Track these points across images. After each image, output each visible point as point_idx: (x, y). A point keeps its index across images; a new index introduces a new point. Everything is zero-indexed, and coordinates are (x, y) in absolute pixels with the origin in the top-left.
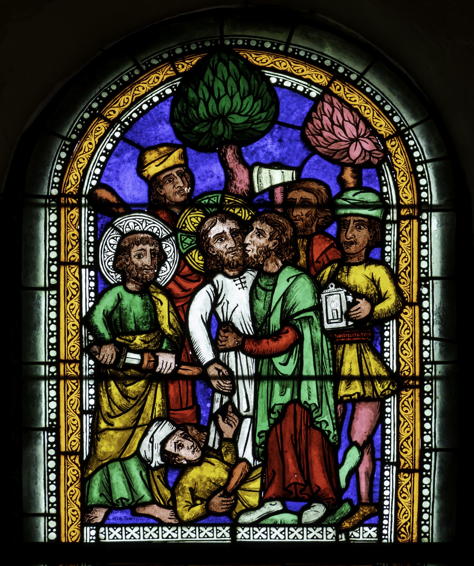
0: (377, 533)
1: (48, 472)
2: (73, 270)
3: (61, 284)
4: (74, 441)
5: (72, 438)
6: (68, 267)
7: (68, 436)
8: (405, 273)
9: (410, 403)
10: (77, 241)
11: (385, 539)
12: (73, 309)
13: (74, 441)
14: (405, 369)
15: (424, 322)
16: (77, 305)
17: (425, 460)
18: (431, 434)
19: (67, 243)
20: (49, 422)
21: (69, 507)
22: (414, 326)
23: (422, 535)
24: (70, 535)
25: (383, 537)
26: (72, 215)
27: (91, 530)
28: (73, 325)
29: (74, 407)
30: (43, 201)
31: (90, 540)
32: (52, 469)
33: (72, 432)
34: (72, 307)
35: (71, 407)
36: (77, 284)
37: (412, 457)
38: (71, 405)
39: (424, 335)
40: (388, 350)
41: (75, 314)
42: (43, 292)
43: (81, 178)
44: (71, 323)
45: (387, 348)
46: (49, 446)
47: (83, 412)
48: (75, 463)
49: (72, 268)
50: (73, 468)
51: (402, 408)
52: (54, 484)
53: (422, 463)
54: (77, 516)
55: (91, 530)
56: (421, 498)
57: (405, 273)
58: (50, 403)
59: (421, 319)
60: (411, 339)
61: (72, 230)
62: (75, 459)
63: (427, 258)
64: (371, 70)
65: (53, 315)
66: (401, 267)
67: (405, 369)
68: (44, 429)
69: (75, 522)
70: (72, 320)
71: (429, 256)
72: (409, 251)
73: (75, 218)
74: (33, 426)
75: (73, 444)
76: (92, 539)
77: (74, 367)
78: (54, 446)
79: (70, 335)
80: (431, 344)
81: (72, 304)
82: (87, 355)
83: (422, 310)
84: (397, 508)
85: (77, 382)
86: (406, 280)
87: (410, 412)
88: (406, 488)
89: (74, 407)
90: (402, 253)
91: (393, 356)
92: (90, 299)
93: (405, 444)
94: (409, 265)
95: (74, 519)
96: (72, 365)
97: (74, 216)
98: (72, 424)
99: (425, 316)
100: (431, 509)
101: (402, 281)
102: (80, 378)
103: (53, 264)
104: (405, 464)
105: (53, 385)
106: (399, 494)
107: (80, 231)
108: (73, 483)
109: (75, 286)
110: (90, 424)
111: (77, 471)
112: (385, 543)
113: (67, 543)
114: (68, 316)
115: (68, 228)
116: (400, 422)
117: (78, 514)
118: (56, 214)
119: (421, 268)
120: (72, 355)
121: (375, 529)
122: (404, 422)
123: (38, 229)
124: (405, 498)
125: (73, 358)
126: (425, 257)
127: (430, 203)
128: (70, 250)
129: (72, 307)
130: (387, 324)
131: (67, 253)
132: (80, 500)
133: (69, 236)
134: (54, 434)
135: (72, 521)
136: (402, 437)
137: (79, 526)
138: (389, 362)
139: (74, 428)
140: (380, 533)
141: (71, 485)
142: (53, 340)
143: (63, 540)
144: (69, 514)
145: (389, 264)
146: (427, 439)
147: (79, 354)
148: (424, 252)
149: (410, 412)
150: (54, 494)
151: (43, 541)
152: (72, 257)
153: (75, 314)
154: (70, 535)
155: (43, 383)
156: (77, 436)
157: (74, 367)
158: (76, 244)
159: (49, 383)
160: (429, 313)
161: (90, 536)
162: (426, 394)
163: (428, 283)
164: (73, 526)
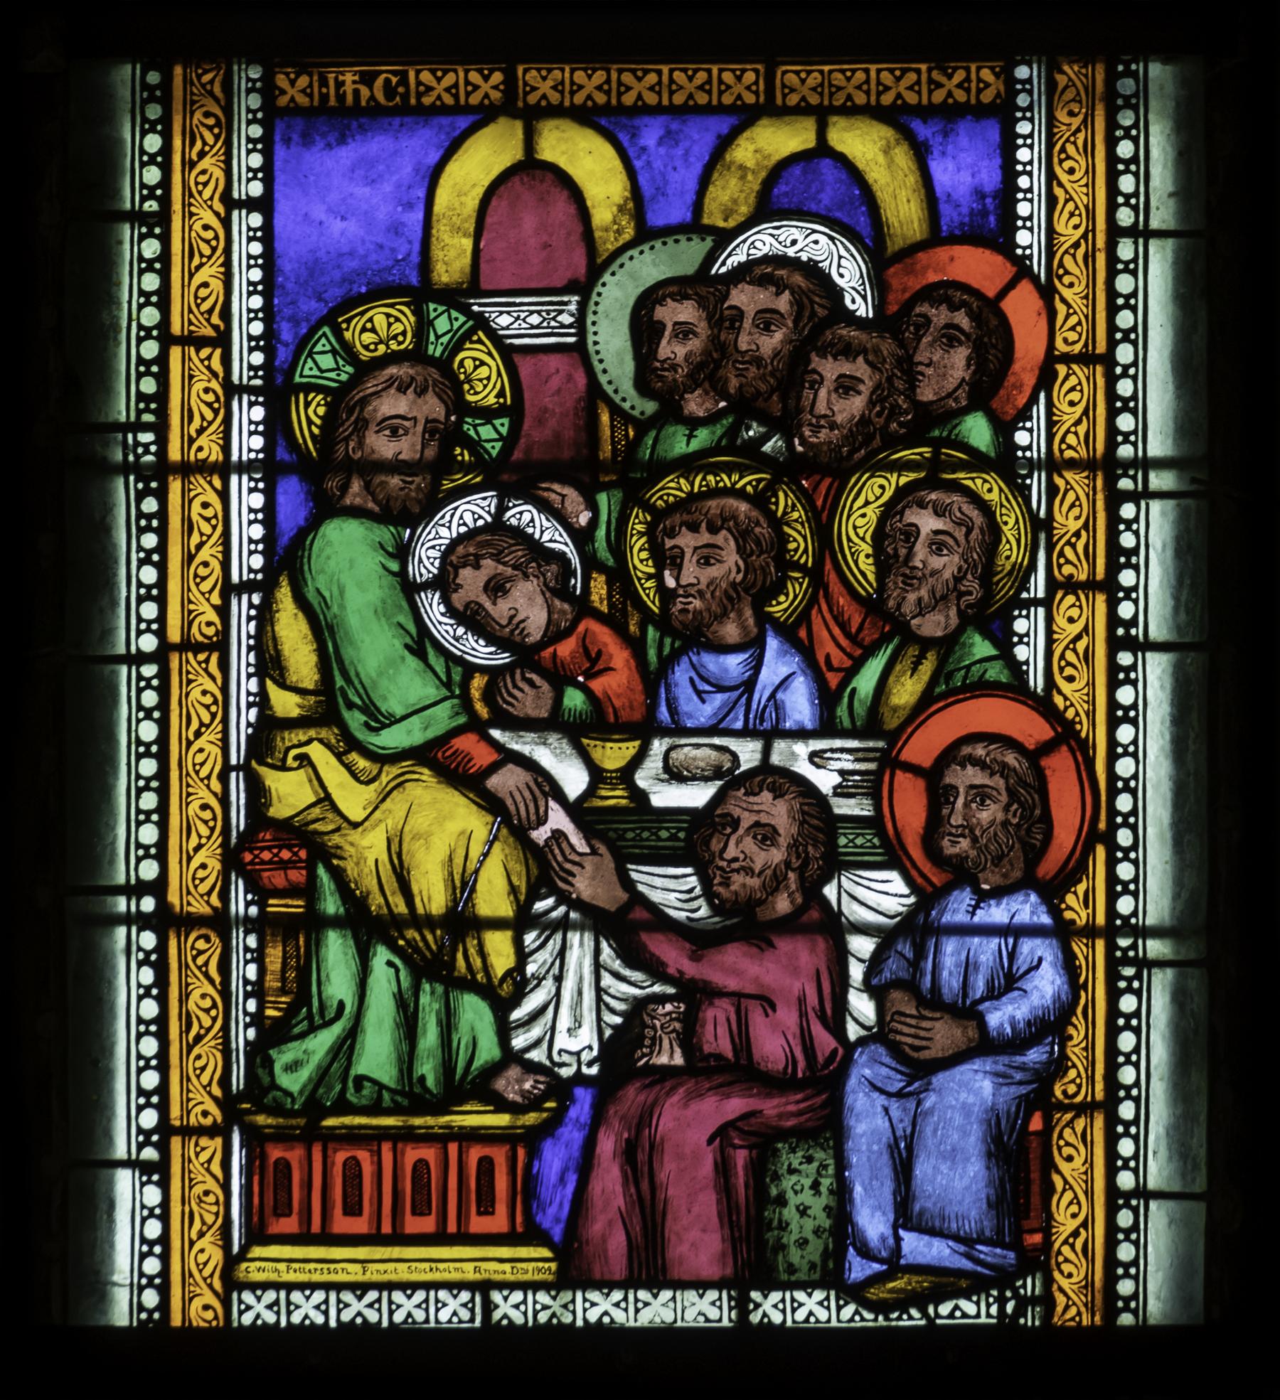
4: (1071, 620)
5: (204, 555)
7: (1088, 531)
9: (1081, 652)
12: (202, 880)
13: (1071, 620)
14: (1068, 1316)
15: (1120, 784)
17: (1122, 984)
18: (1137, 205)
20: (138, 1097)
21: (192, 494)
22: (183, 966)
23: (1120, 1163)
27: (251, 405)
29: (205, 1078)
30: (121, 904)
31: (250, 378)
33: (198, 540)
37: (1086, 297)
39: (1119, 954)
42: (124, 669)
44: (199, 1109)
45: (1025, 219)
46: (142, 1028)
47: (229, 589)
50: (1073, 178)
52: (1121, 295)
54: (214, 522)
55: (251, 405)
57: (1072, 1247)
61: (198, 983)
63: (1133, 405)
65: (151, 1080)
67: (1068, 1316)
71: (1141, 261)
72: (1086, 706)
73: (206, 1065)
76: (256, 377)
77: (209, 358)
79: (1081, 652)
80: (1142, 189)
81: (1074, 1216)
84: (1052, 201)
86: (1075, 566)
87: (1078, 1161)
88: (1075, 650)
91: (1039, 195)
94: (1084, 1225)
95: (1071, 439)
96: (205, 352)
97: (204, 755)
98: (201, 819)
99: (150, 316)
100: (1142, 199)
101: (1066, 1268)
102: (224, 469)
103: (150, 1253)
104: (1067, 1307)
106: (1056, 160)
110: (249, 725)
111: (213, 695)
113: (188, 1331)
118: (155, 998)
120: (201, 587)
123: (116, 355)
124: (1071, 679)
126: (1129, 434)
133: (191, 813)
134: (155, 1178)
139: (206, 529)
141: (201, 431)
143: (176, 1321)
144: (195, 517)
146: (151, 248)
148: (1125, 695)
150: (155, 333)
155: (127, 229)
157: (209, 358)
159: (138, 673)
161: (251, 422)
163: (1134, 67)
164: (203, 852)
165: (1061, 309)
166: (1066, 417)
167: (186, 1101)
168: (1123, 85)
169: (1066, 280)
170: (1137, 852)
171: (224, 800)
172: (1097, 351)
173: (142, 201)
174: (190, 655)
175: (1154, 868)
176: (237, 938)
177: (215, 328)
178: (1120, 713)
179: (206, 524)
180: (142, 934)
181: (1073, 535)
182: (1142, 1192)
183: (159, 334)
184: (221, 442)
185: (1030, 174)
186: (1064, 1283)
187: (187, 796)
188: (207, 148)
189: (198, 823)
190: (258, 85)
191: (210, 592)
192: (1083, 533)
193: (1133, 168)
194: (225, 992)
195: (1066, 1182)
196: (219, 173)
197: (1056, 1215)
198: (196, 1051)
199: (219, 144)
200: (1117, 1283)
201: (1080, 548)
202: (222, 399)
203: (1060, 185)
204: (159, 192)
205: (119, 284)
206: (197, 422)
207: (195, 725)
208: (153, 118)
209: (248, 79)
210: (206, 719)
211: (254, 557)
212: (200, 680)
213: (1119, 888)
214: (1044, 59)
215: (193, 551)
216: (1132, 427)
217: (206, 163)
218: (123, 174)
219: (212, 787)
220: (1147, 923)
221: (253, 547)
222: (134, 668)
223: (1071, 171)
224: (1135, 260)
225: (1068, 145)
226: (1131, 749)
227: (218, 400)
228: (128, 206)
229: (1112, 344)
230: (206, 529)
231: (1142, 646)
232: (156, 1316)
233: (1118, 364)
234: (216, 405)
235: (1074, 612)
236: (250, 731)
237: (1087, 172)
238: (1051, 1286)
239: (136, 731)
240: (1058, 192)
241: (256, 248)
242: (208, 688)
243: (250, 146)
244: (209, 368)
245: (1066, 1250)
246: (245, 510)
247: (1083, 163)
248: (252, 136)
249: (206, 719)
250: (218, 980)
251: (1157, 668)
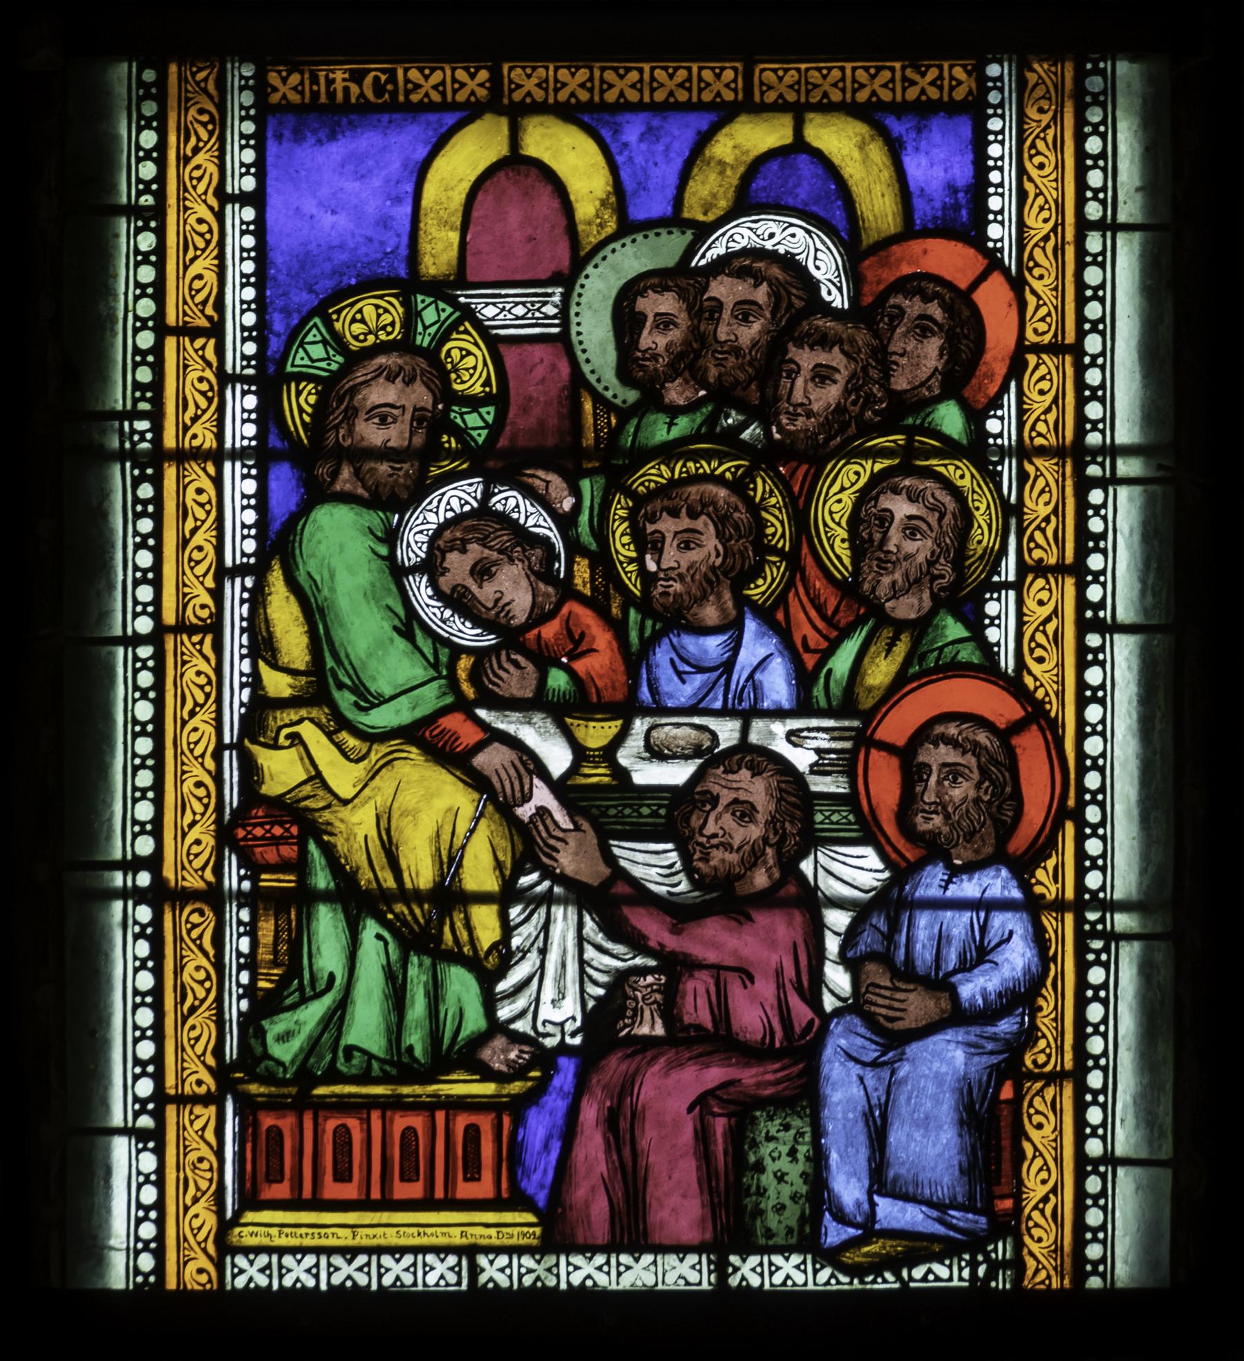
7: (1057, 517)
9: (1050, 634)
12: (197, 855)
14: (1038, 1279)
15: (1088, 762)
17: (1091, 957)
18: (1105, 200)
20: (134, 1067)
21: (187, 480)
22: (178, 939)
23: (1088, 1131)
27: (244, 393)
29: (199, 1048)
30: (118, 879)
31: (243, 368)
33: (193, 525)
38: (192, 1042)
39: (1087, 927)
42: (120, 651)
43: (215, 965)
44: (193, 1078)
45: (996, 213)
46: (138, 1000)
47: (222, 573)
52: (1089, 287)
54: (208, 507)
55: (244, 393)
57: (1042, 1212)
61: (193, 956)
63: (1101, 394)
65: (146, 1049)
67: (1038, 1279)
71: (1109, 254)
72: (1055, 686)
76: (248, 366)
77: (203, 348)
80: (1110, 184)
81: (1044, 1182)
84: (1022, 196)
87: (1048, 1129)
88: (1044, 632)
91: (1010, 190)
94: (1054, 1190)
95: (1041, 427)
96: (199, 342)
97: (198, 734)
98: (195, 796)
99: (146, 307)
100: (1110, 193)
101: (1036, 1232)
102: (218, 456)
103: (146, 1218)
104: (1037, 1271)
106: (1026, 156)
107: (218, 778)
109: (202, 680)
110: (242, 704)
111: (207, 676)
113: (183, 1294)
118: (150, 970)
120: (195, 571)
123: (112, 345)
124: (1040, 660)
126: (1097, 422)
133: (185, 790)
134: (151, 1145)
139: (201, 514)
141: (195, 419)
143: (171, 1284)
144: (189, 503)
148: (1093, 676)
150: (150, 324)
155: (123, 222)
157: (203, 348)
159: (135, 654)
161: (244, 410)
163: (1102, 65)
164: (197, 828)
165: (1031, 301)
166: (1036, 406)
167: (180, 1071)
168: (1092, 83)
169: (1036, 272)
170: (1105, 829)
172: (1067, 342)
173: (138, 196)
175: (1121, 844)
176: (231, 912)
177: (209, 318)
178: (1088, 693)
179: (201, 510)
180: (138, 908)
181: (1043, 520)
182: (1110, 1159)
183: (155, 325)
184: (215, 430)
185: (1001, 169)
186: (1035, 1247)
187: (182, 774)
188: (201, 144)
189: (193, 800)
190: (251, 82)
191: (204, 575)
192: (1053, 518)
193: (1101, 163)
194: (219, 965)
195: (1036, 1149)
196: (212, 169)
197: (1026, 1182)
198: (190, 1022)
199: (213, 140)
200: (1085, 1247)
201: (1050, 533)
202: (216, 388)
203: (1031, 180)
204: (154, 187)
205: (115, 276)
206: (191, 411)
207: (189, 704)
209: (241, 77)
210: (201, 699)
211: (247, 541)
212: (195, 661)
213: (1088, 863)
214: (1015, 57)
215: (188, 536)
216: (1100, 415)
217: (200, 158)
218: (120, 169)
219: (206, 765)
220: (1115, 897)
221: (246, 532)
222: (130, 650)
223: (1041, 166)
224: (1103, 253)
225: (1038, 141)
226: (1100, 728)
227: (211, 389)
228: (124, 200)
229: (1081, 335)
230: (201, 514)
231: (1110, 628)
232: (152, 1279)
233: (1086, 354)
234: (210, 394)
235: (1044, 595)
236: (243, 710)
237: (1056, 167)
238: (1021, 1251)
239: (133, 710)
240: (1029, 186)
241: (249, 241)
242: (202, 669)
243: (243, 142)
244: (203, 358)
246: (238, 496)
247: (1053, 159)
248: (245, 132)
249: (201, 699)
250: (212, 953)
251: (1124, 650)
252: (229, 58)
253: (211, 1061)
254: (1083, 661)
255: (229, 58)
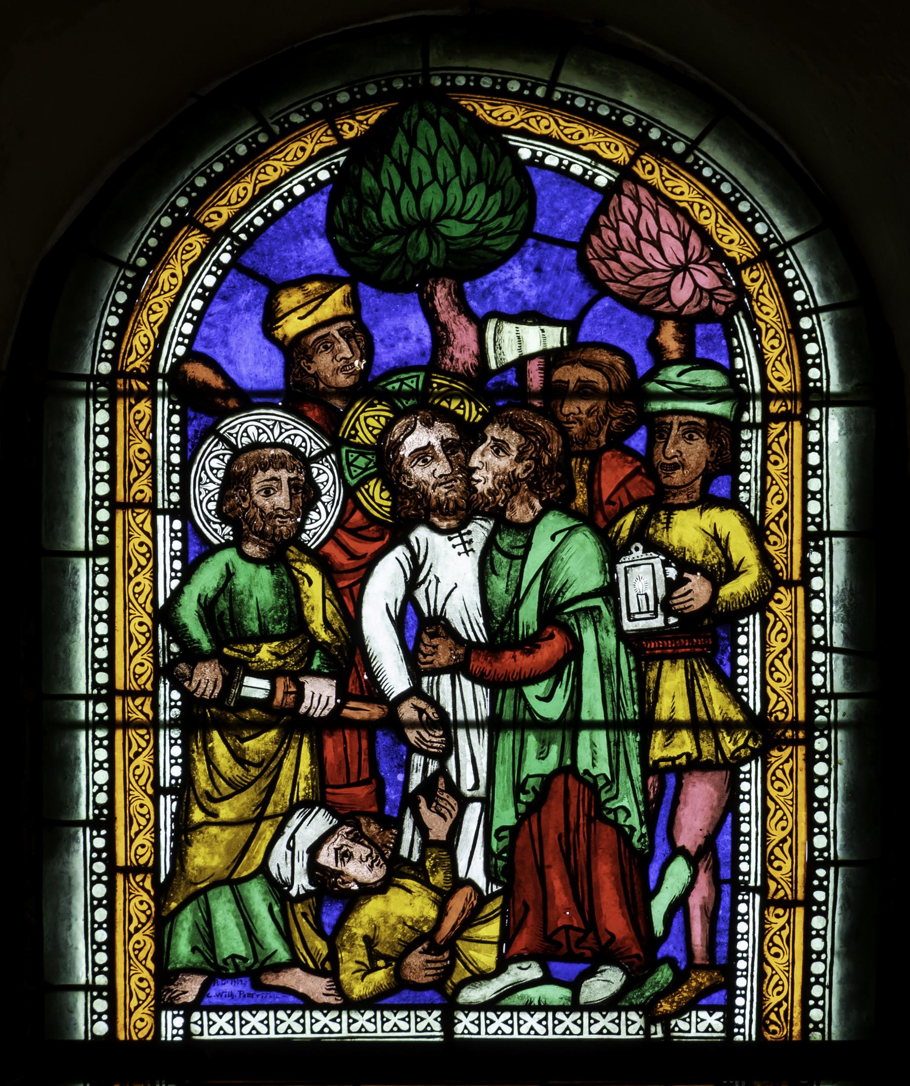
0: (723, 1023)
1: (92, 905)
2: (139, 519)
3: (117, 545)
4: (143, 846)
6: (130, 512)
7: (130, 837)
8: (777, 523)
9: (787, 772)
10: (148, 462)
11: (739, 1033)
12: (140, 594)
13: (143, 846)
14: (777, 708)
15: (814, 618)
16: (147, 585)
17: (816, 883)
18: (828, 832)
19: (128, 466)
20: (94, 810)
21: (132, 972)
22: (794, 625)
24: (135, 1027)
25: (736, 1030)
26: (139, 412)
27: (174, 1016)
28: (141, 624)
29: (142, 781)
30: (83, 386)
31: (173, 1036)
32: (100, 900)
33: (137, 829)
34: (137, 590)
35: (137, 781)
36: (147, 545)
38: (137, 778)
39: (814, 642)
40: (746, 671)
41: (145, 603)
42: (83, 561)
44: (137, 620)
45: (743, 668)
46: (95, 855)
47: (158, 791)
48: (143, 888)
49: (138, 514)
50: (140, 899)
51: (772, 782)
52: (104, 929)
53: (809, 889)
54: (148, 991)
55: (174, 1016)
56: (809, 956)
57: (777, 523)
58: (97, 773)
59: (808, 612)
60: (788, 650)
61: (138, 441)
62: (143, 880)
63: (820, 496)
64: (713, 134)
65: (102, 604)
66: (769, 511)
67: (777, 708)
68: (85, 824)
69: (144, 1001)
70: (138, 614)
71: (825, 492)
72: (786, 482)
73: (143, 418)
74: (64, 818)
75: (141, 851)
76: (177, 1035)
77: (142, 704)
78: (104, 855)
80: (828, 660)
81: (138, 584)
82: (167, 682)
83: (811, 594)
84: (762, 975)
85: (148, 733)
87: (786, 791)
88: (780, 936)
89: (142, 781)
90: (772, 485)
91: (755, 682)
92: (173, 574)
93: (777, 851)
94: (786, 508)
95: (142, 995)
96: (139, 701)
97: (141, 415)
99: (817, 606)
101: (772, 538)
102: (154, 725)
103: (101, 506)
104: (777, 890)
105: (101, 740)
106: (765, 948)
108: (140, 926)
110: (172, 813)
111: (148, 903)
112: (739, 1042)
113: (129, 1043)
114: (131, 606)
115: (131, 438)
116: (768, 810)
117: (149, 987)
118: (107, 410)
119: (808, 515)
120: (139, 681)
121: (719, 1014)
122: (776, 810)
123: (73, 439)
124: (777, 955)
125: (139, 686)
126: (816, 493)
127: (825, 389)
128: (135, 480)
129: (137, 590)
130: (743, 622)
131: (128, 486)
132: (153, 959)
134: (103, 832)
135: (139, 1000)
136: (773, 838)
137: (152, 1009)
138: (747, 695)
139: (143, 821)
140: (729, 1023)
141: (137, 930)
142: (102, 653)
143: (121, 1036)
144: (133, 986)
145: (747, 506)
147: (152, 678)
148: (814, 484)
149: (786, 791)
150: (104, 948)
151: (82, 1037)
152: (139, 494)
153: (145, 603)
154: (135, 1027)
155: (82, 735)
156: (148, 836)
157: (142, 704)
158: (147, 468)
159: (94, 734)
160: (823, 600)
161: (174, 1028)
162: (817, 757)
163: (821, 543)
164: (140, 1009)
171: (153, 443)
174: (130, 700)
208: (101, 963)
240: (771, 804)
245: (773, 526)
252: (158, 1081)
253: (149, 609)
254: (807, 495)
255: (158, 1081)
